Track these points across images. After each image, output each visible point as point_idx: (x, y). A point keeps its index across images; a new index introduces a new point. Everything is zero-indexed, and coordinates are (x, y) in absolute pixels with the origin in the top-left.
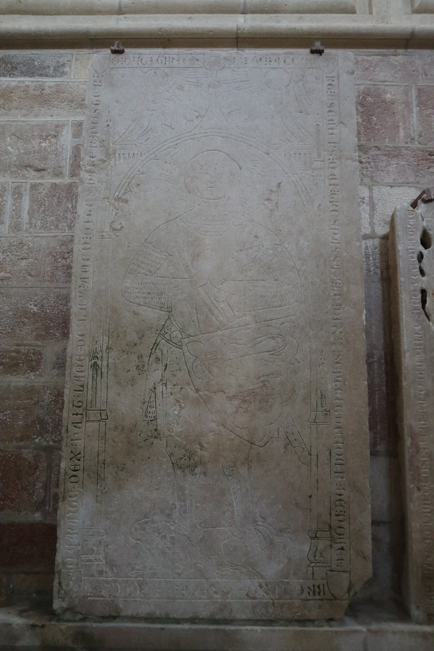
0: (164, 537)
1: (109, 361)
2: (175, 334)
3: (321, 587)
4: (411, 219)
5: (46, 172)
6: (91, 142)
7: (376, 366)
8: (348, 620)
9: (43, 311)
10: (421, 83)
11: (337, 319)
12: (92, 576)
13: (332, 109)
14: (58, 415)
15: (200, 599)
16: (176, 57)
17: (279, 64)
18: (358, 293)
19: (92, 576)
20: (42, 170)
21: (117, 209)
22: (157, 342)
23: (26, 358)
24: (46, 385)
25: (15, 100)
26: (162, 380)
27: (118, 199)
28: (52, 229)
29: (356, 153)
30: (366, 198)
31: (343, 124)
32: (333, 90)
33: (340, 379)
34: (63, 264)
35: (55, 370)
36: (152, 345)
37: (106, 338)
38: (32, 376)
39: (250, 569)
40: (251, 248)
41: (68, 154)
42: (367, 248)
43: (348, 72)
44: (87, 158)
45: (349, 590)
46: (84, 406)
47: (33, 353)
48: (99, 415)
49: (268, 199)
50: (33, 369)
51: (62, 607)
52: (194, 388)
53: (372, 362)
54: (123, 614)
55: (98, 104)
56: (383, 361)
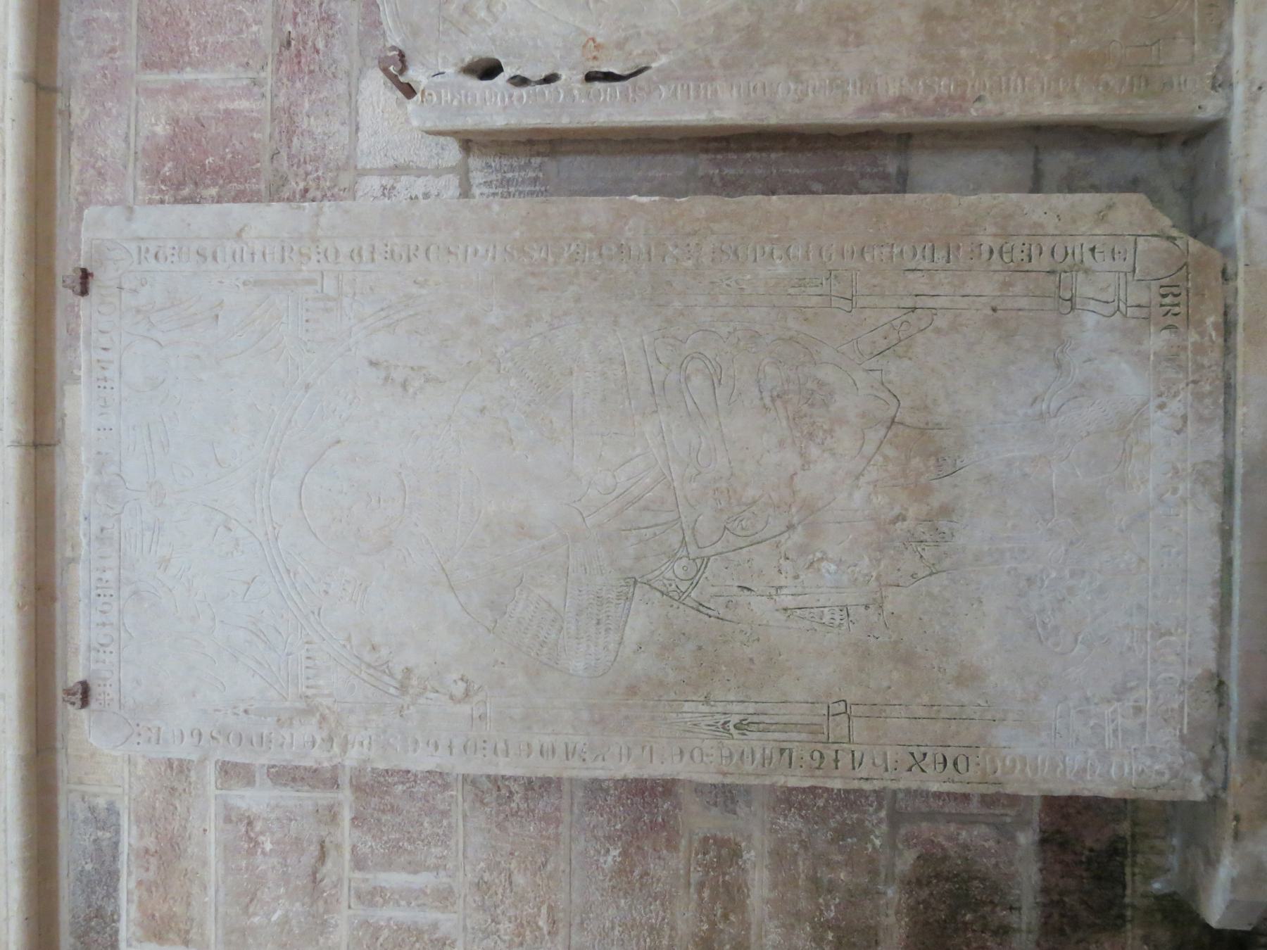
0: (1071, 590)
1: (733, 698)
2: (679, 572)
3: (1163, 291)
4: (439, 98)
5: (327, 840)
6: (282, 745)
7: (729, 171)
8: (1224, 240)
9: (620, 837)
10: (132, 63)
11: (649, 253)
12: (1143, 725)
13: (209, 254)
14: (827, 801)
15: (1186, 521)
16: (95, 575)
17: (111, 362)
18: (596, 210)
19: (1143, 725)
20: (322, 847)
21: (425, 689)
22: (695, 605)
23: (714, 869)
24: (768, 826)
25: (170, 908)
26: (770, 596)
27: (403, 688)
28: (450, 824)
29: (304, 208)
30: (384, 182)
31: (242, 230)
32: (169, 252)
33: (767, 249)
34: (520, 799)
35: (738, 809)
36: (701, 616)
37: (687, 707)
38: (749, 855)
39: (1131, 425)
40: (506, 422)
41: (289, 796)
42: (488, 184)
43: (129, 219)
44: (316, 752)
45: (1171, 239)
46: (819, 746)
47: (705, 854)
48: (837, 718)
49: (404, 386)
50: (736, 854)
51: (1202, 785)
52: (786, 535)
53: (722, 178)
54: (1213, 667)
55: (200, 734)
56: (719, 157)
